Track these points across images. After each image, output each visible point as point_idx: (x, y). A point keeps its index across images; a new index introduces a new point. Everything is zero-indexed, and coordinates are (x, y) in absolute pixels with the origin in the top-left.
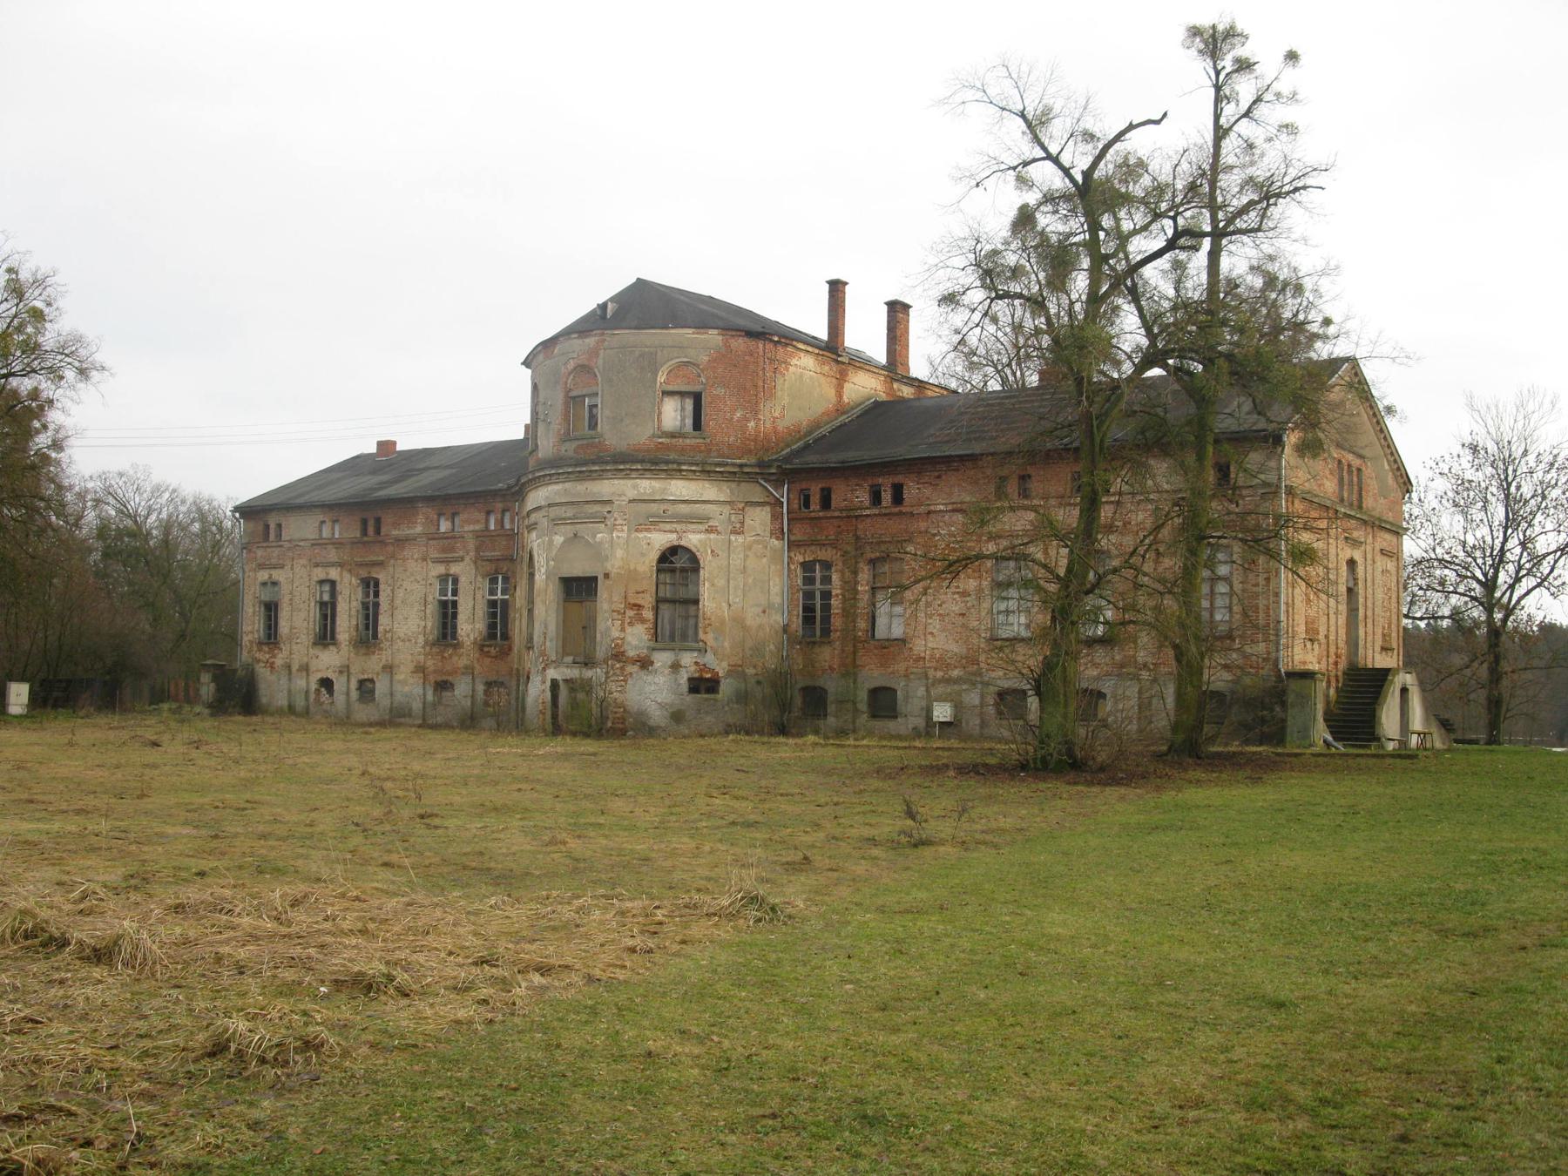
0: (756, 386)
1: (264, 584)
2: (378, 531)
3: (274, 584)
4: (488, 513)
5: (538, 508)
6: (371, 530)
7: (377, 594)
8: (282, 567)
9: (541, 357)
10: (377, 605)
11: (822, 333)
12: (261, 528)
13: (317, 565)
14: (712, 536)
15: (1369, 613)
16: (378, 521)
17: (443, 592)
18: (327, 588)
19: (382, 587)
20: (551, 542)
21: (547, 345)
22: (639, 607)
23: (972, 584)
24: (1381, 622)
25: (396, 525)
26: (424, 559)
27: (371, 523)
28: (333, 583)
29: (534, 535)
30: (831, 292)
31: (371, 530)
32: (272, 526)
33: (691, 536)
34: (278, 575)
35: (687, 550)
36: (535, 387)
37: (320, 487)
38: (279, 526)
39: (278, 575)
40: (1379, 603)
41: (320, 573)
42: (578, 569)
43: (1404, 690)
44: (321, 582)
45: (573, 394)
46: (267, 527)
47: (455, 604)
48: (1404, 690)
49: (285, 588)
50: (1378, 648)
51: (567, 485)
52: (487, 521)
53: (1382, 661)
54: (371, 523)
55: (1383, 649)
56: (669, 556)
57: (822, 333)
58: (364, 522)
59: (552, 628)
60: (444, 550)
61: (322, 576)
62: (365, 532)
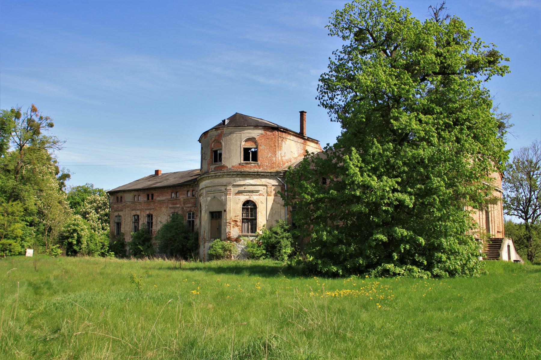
0: (275, 146)
1: (116, 216)
2: (152, 198)
3: (120, 216)
4: (188, 191)
5: (202, 189)
6: (150, 198)
7: (152, 219)
8: (122, 211)
9: (203, 138)
10: (152, 223)
11: (298, 131)
12: (115, 198)
13: (133, 210)
14: (261, 197)
15: (493, 219)
16: (152, 195)
17: (189, 217)
18: (136, 217)
19: (153, 217)
20: (207, 199)
21: (205, 133)
22: (236, 221)
23: (268, 233)
24: (497, 222)
25: (158, 196)
26: (167, 207)
27: (150, 196)
28: (138, 216)
29: (201, 198)
30: (301, 115)
31: (150, 198)
32: (119, 197)
33: (254, 197)
34: (121, 213)
35: (253, 202)
36: (202, 148)
37: (136, 184)
38: (121, 197)
39: (121, 213)
40: (496, 215)
41: (134, 213)
42: (215, 209)
43: (509, 246)
44: (134, 216)
45: (214, 150)
46: (118, 198)
47: (193, 221)
48: (509, 246)
49: (123, 217)
50: (496, 232)
51: (212, 180)
52: (187, 194)
53: (500, 236)
54: (150, 196)
55: (498, 232)
56: (247, 203)
57: (298, 131)
58: (148, 195)
59: (207, 228)
60: (173, 204)
61: (135, 214)
62: (148, 199)
